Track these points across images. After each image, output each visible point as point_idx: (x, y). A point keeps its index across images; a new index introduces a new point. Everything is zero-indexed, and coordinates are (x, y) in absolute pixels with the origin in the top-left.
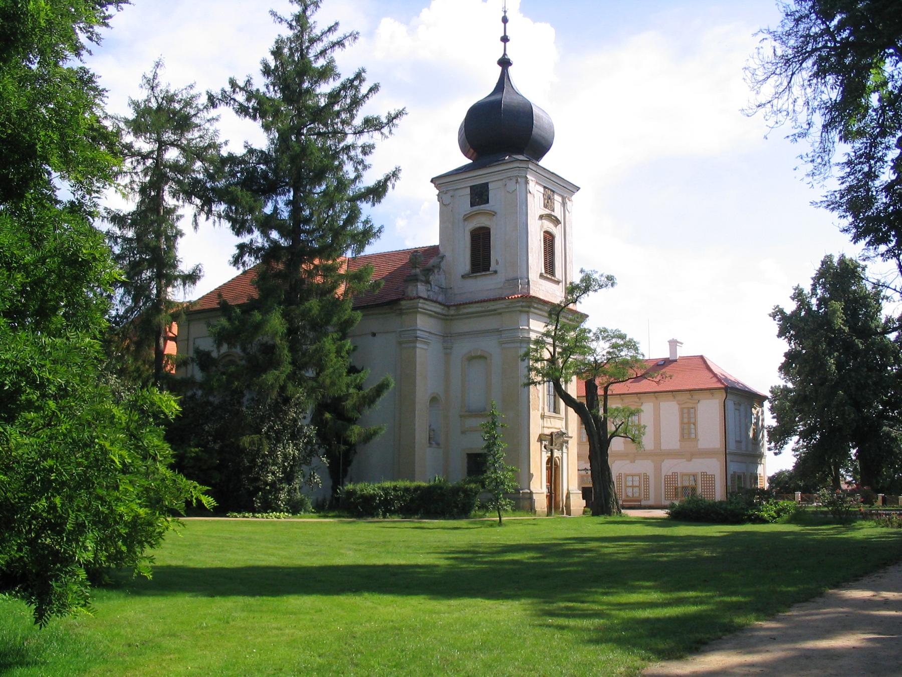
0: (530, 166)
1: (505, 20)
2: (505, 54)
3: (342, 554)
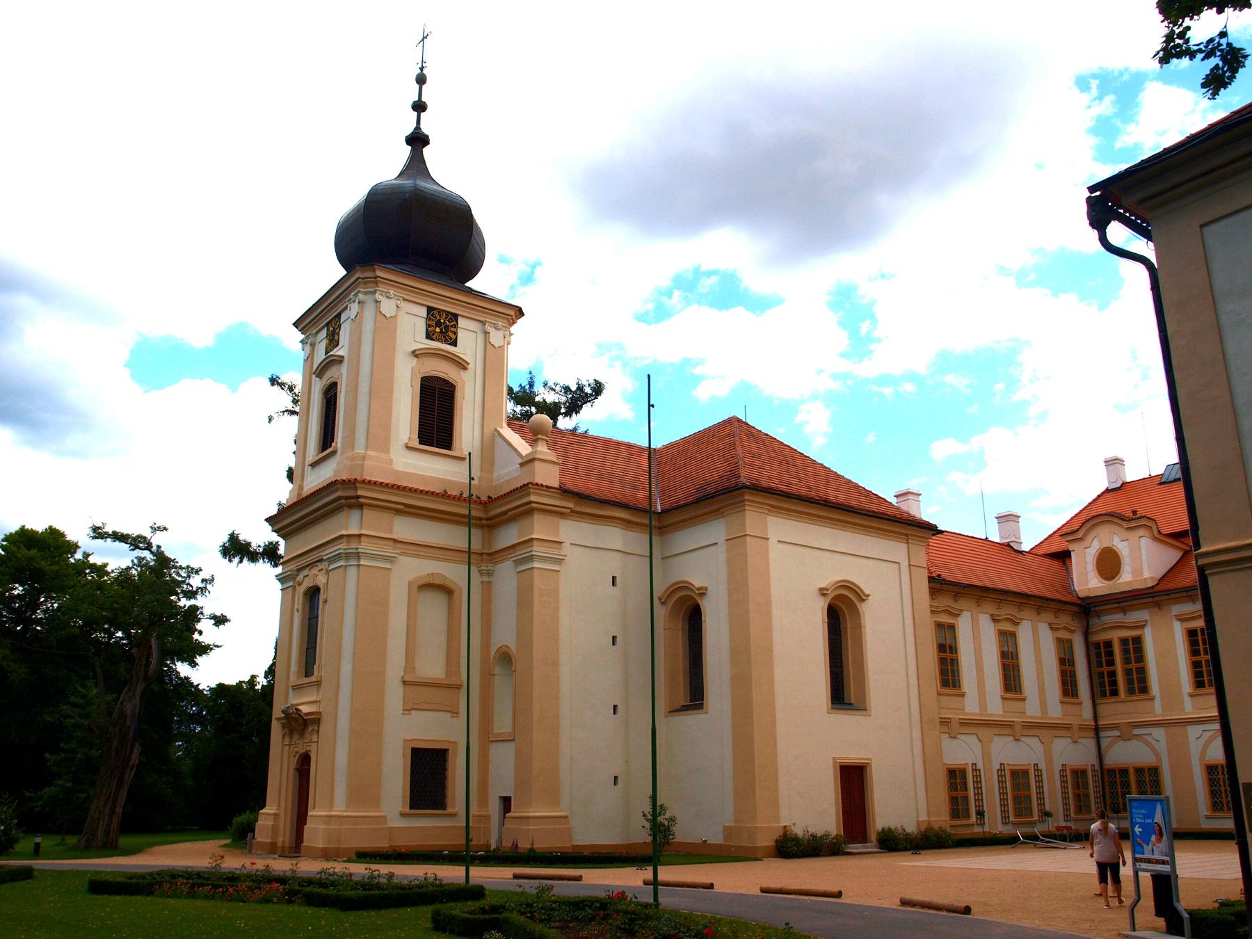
0: (379, 273)
1: (421, 80)
2: (418, 128)
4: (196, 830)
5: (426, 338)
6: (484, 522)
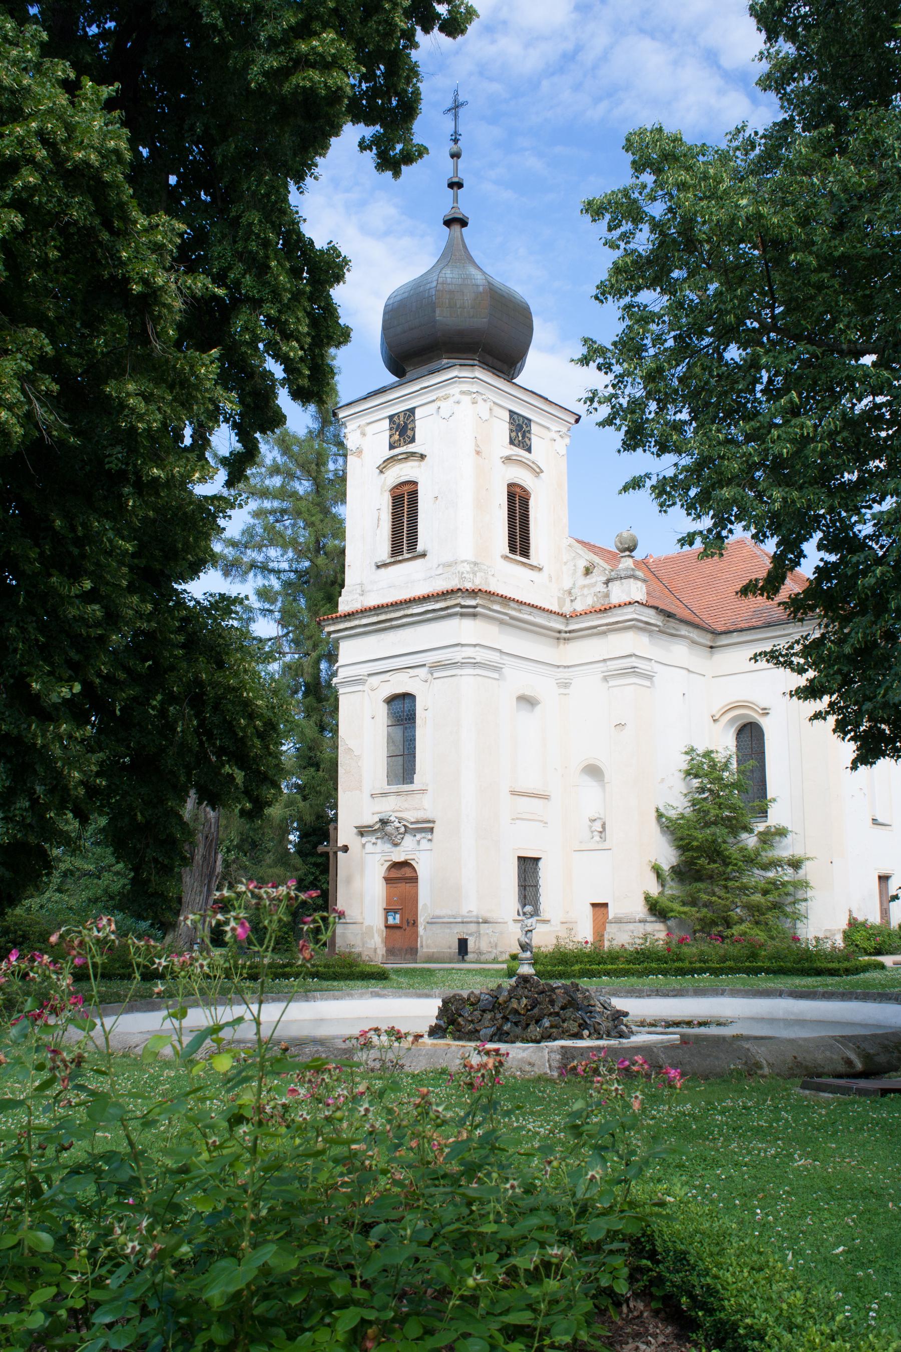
5: (415, 483)
6: (564, 635)
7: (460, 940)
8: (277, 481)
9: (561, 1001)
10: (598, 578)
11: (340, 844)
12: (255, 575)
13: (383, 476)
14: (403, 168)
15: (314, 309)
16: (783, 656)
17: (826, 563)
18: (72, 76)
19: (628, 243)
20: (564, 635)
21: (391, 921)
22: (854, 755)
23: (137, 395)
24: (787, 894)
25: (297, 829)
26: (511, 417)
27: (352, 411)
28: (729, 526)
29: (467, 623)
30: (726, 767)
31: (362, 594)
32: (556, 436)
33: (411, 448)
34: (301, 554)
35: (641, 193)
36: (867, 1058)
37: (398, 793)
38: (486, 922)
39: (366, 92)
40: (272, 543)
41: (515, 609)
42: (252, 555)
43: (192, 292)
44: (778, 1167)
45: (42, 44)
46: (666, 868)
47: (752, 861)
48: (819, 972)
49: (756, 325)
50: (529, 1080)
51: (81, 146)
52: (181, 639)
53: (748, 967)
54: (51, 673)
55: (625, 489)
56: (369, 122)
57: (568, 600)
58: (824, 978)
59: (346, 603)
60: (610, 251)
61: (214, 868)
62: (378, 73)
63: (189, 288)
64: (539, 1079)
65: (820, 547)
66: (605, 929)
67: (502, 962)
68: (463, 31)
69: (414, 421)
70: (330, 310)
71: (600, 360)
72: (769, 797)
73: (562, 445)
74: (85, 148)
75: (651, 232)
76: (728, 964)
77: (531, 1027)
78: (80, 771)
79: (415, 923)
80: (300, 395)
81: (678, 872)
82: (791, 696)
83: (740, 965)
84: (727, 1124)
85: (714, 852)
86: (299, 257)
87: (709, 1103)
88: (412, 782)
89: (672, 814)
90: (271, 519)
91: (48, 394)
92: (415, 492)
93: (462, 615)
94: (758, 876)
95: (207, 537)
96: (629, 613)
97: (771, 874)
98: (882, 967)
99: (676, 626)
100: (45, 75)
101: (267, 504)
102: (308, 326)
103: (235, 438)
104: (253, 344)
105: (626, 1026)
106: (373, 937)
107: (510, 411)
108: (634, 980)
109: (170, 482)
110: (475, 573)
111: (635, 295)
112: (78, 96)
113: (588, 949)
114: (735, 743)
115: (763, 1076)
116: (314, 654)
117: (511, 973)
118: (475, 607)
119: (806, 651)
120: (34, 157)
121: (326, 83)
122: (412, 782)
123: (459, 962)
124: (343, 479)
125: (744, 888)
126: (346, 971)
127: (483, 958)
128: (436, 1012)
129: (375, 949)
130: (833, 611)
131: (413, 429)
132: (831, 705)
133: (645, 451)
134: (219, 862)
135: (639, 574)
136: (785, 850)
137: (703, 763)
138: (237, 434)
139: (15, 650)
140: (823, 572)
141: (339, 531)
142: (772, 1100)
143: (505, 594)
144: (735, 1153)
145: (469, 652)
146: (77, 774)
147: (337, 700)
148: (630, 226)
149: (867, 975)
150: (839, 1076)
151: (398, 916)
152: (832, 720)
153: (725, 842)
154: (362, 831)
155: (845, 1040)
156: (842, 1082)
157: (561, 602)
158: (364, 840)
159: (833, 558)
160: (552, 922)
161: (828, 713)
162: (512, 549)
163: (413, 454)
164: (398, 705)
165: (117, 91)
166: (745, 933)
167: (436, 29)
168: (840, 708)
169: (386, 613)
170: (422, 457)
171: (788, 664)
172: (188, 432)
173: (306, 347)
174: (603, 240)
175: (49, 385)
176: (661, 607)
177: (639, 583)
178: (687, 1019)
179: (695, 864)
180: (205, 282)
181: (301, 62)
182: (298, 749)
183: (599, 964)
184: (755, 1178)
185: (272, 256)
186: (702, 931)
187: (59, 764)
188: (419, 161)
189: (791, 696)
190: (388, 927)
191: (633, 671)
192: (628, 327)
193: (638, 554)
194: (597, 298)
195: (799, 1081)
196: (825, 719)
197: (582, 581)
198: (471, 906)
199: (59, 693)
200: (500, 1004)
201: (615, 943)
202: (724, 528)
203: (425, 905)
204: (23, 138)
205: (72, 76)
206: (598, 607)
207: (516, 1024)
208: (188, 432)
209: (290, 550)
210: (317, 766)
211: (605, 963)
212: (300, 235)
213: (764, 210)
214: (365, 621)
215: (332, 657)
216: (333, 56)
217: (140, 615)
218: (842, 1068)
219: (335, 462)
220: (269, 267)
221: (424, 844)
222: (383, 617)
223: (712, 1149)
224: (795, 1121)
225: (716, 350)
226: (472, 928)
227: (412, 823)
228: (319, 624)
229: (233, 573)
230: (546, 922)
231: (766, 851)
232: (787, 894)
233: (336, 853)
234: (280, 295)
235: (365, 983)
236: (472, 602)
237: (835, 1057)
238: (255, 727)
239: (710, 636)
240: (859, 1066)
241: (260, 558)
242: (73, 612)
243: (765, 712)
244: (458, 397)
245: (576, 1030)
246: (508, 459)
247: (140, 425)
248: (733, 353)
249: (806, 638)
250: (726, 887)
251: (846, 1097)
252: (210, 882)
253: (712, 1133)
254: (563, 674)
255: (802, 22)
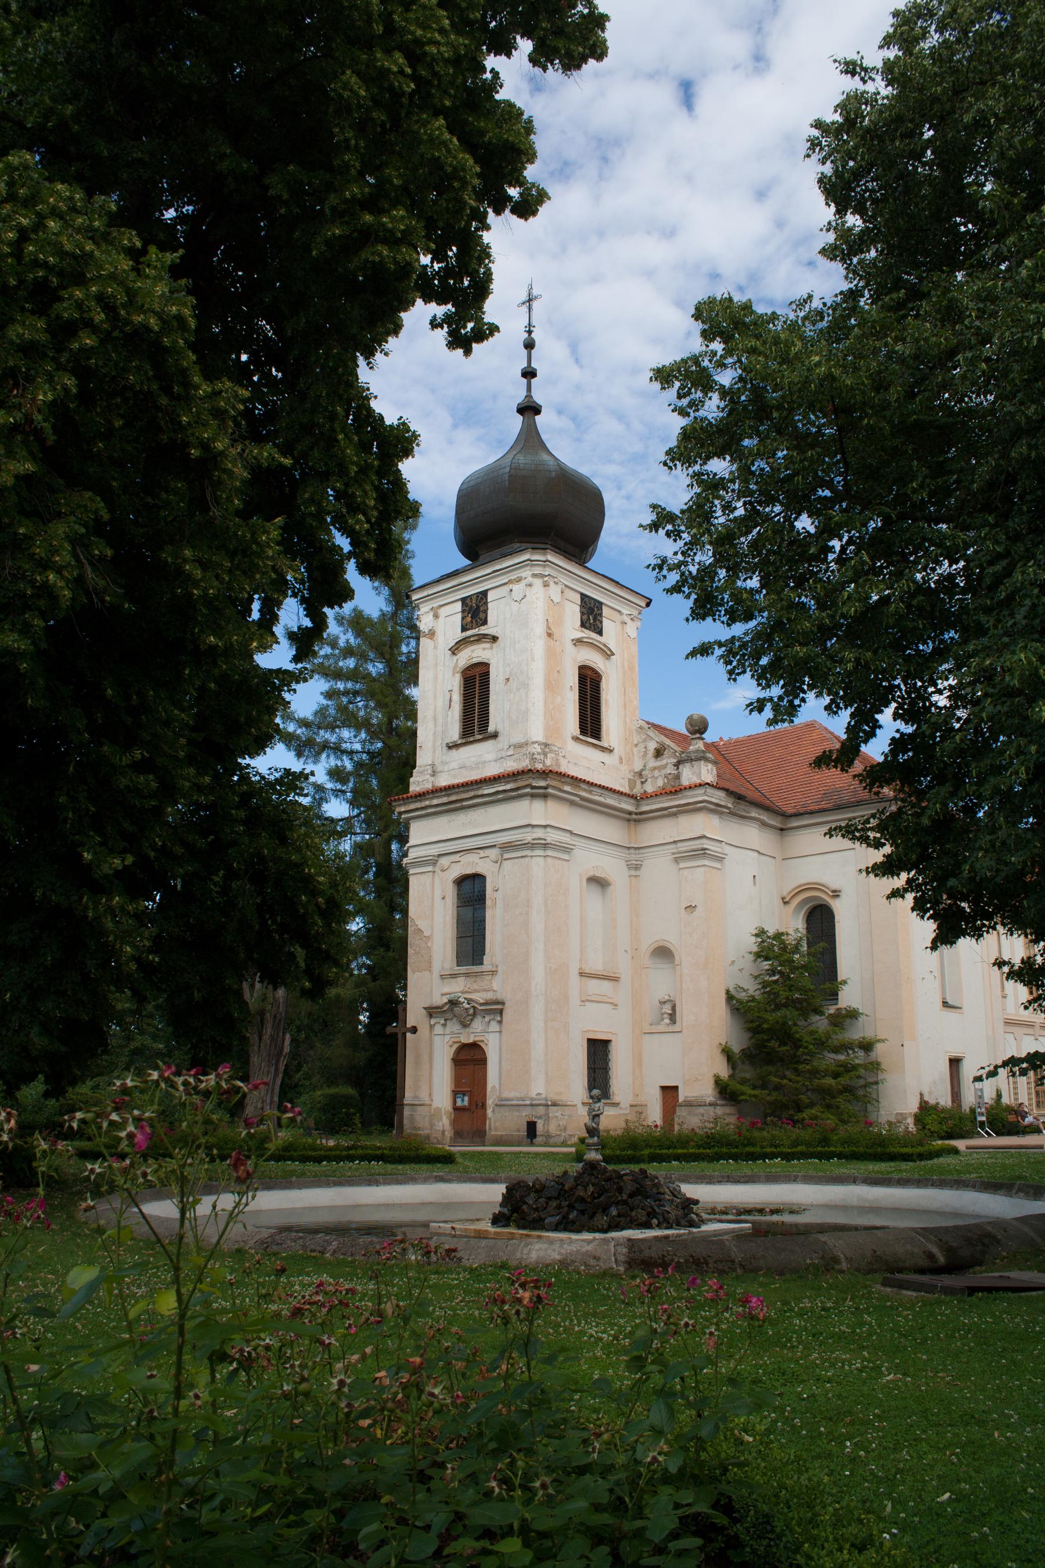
1: (529, 345)
2: (529, 396)
3: (1010, 598)
4: (648, 1146)
5: (486, 665)
6: (634, 816)
7: (528, 1123)
8: (351, 663)
9: (629, 1187)
10: (668, 760)
11: (409, 1025)
12: (328, 756)
13: (455, 658)
14: (474, 345)
15: (383, 484)
16: (858, 831)
17: (902, 734)
18: (139, 244)
19: (697, 410)
20: (634, 816)
21: (459, 1103)
22: (933, 935)
23: (193, 561)
24: (859, 1077)
25: (367, 1010)
26: (582, 600)
27: (425, 593)
28: (802, 695)
29: (538, 805)
30: (796, 949)
31: (434, 774)
32: (627, 619)
33: (483, 630)
34: (373, 735)
35: (710, 361)
36: (950, 1251)
37: (467, 975)
38: (554, 1104)
39: (437, 273)
40: (344, 725)
41: (585, 790)
42: (324, 735)
43: (258, 461)
44: (864, 1383)
45: (110, 213)
46: (736, 1049)
47: (823, 1043)
48: (892, 1158)
49: (827, 493)
50: (593, 1276)
51: (141, 309)
52: (242, 814)
53: (820, 1153)
54: (101, 844)
55: (693, 654)
56: (441, 301)
57: (638, 782)
58: (898, 1163)
59: (418, 782)
60: (680, 418)
61: (282, 1048)
62: (450, 254)
63: (255, 458)
64: (605, 1274)
65: (896, 716)
66: (675, 1112)
67: (571, 1146)
68: (534, 213)
69: (486, 603)
70: (399, 485)
71: (669, 527)
72: (839, 980)
73: (632, 629)
74: (145, 313)
75: (721, 399)
76: (799, 1148)
77: (598, 1216)
78: (133, 945)
79: (484, 1106)
80: (365, 569)
81: (748, 1055)
82: (868, 873)
83: (811, 1149)
84: (806, 1329)
85: (784, 1034)
86: (369, 432)
87: (785, 1303)
88: (482, 963)
89: (742, 996)
90: (345, 700)
91: (102, 558)
92: (487, 674)
93: (533, 796)
94: (831, 1059)
95: (272, 713)
96: (698, 795)
97: (842, 1057)
98: (955, 1151)
99: (746, 808)
100: (112, 243)
101: (340, 686)
102: (375, 499)
103: (302, 612)
104: (319, 516)
105: (697, 1215)
106: (441, 1119)
107: (582, 595)
108: (704, 1164)
109: (228, 652)
110: (545, 755)
111: (705, 463)
112: (142, 263)
113: (658, 1132)
114: (805, 926)
115: (841, 1271)
116: (385, 835)
117: (579, 1157)
118: (546, 788)
119: (880, 828)
120: (92, 320)
121: (394, 258)
122: (482, 963)
123: (527, 1145)
124: (416, 662)
125: (815, 1073)
126: (412, 1154)
127: (551, 1141)
128: (500, 1198)
129: (443, 1132)
130: (910, 784)
131: (486, 612)
132: (909, 881)
133: (714, 620)
134: (287, 1042)
135: (709, 755)
136: (856, 1033)
137: (773, 945)
138: (305, 609)
139: (65, 820)
140: (898, 744)
141: (410, 710)
142: (852, 1299)
143: (575, 774)
144: (817, 1366)
145: (539, 833)
146: (128, 949)
147: (407, 881)
148: (699, 394)
149: (941, 1159)
150: (922, 1271)
151: (466, 1098)
152: (910, 897)
153: (795, 1024)
154: (432, 1012)
155: (925, 1232)
156: (925, 1278)
157: (632, 783)
158: (433, 1021)
159: (909, 729)
160: (621, 1105)
161: (906, 890)
162: (583, 730)
163: (485, 636)
164: (467, 886)
165: (182, 258)
166: (816, 1118)
167: (507, 211)
168: (919, 885)
169: (456, 793)
170: (494, 639)
171: (864, 840)
172: (256, 606)
173: (373, 520)
174: (672, 407)
175: (102, 549)
176: (732, 789)
177: (710, 766)
178: (759, 1206)
179: (766, 1047)
180: (272, 451)
181: (367, 236)
182: (368, 930)
183: (669, 1148)
184: (840, 1396)
185: (338, 429)
186: (773, 1114)
187: (111, 938)
188: (490, 339)
189: (868, 873)
190: (456, 1109)
191: (703, 853)
192: (698, 495)
193: (710, 736)
194: (665, 464)
195: (879, 1277)
196: (903, 897)
197: (652, 763)
198: (538, 1088)
199: (110, 864)
200: (565, 1191)
201: (685, 1126)
202: (796, 696)
203: (494, 1087)
204: (83, 301)
205: (139, 244)
206: (669, 788)
207: (582, 1212)
208: (256, 606)
209: (363, 732)
210: (387, 947)
211: (675, 1147)
212: (370, 411)
213: (836, 372)
214: (435, 802)
215: (403, 839)
216: (402, 232)
217: (199, 788)
218: (923, 1262)
219: (408, 645)
220: (337, 441)
221: (494, 1026)
222: (453, 798)
223: (790, 1360)
224: (879, 1325)
225: (787, 518)
226: (541, 1110)
227: (482, 1004)
228: (390, 804)
229: (306, 753)
230: (616, 1105)
231: (836, 1034)
232: (859, 1077)
233: (404, 1035)
234: (346, 468)
235: (430, 1166)
236: (542, 783)
237: (916, 1250)
238: (317, 905)
239: (780, 818)
240: (942, 1260)
241: (333, 739)
242: (123, 782)
243: (836, 894)
244: (530, 579)
245: (644, 1219)
246: (577, 642)
247: (195, 592)
248: (805, 523)
249: (882, 812)
250: (796, 1070)
251: (931, 1296)
252: (277, 1062)
253: (790, 1340)
254: (633, 856)
255: (870, 196)
